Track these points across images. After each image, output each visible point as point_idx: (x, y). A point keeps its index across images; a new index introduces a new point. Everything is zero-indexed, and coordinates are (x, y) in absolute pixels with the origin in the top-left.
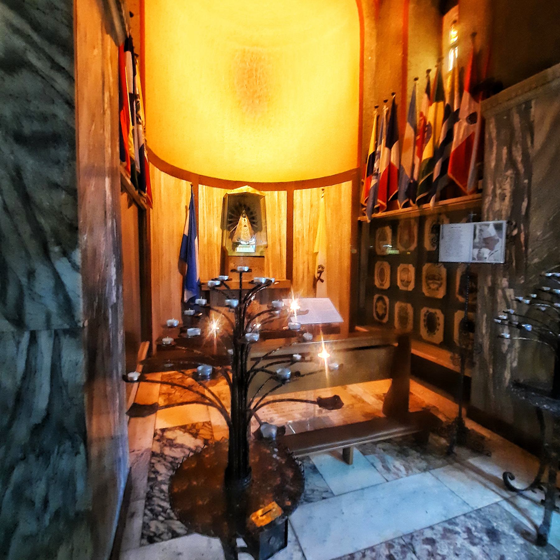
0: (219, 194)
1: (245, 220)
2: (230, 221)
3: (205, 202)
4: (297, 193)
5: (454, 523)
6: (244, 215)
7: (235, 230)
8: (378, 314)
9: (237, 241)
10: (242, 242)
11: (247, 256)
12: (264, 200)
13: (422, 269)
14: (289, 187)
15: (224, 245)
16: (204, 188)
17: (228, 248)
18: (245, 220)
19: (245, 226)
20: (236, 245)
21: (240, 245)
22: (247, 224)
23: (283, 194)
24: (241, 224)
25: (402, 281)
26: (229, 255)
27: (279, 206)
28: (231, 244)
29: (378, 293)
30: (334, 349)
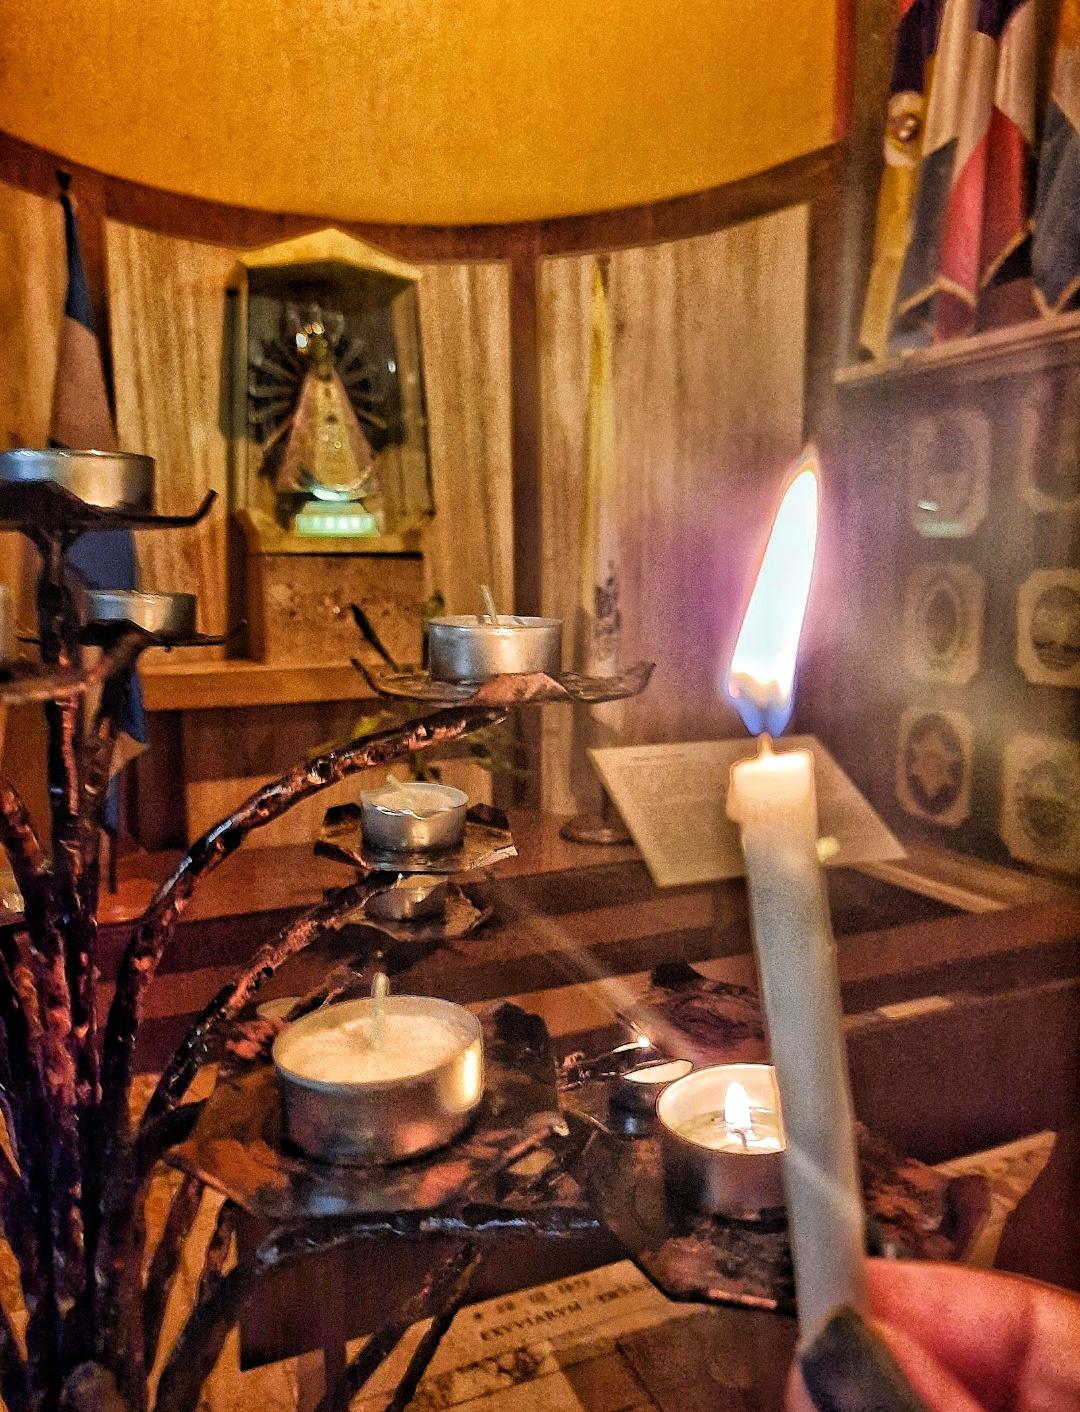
0: (207, 266)
1: (328, 393)
2: (263, 400)
3: (139, 304)
4: (557, 273)
5: (844, 497)
6: (323, 369)
7: (284, 438)
8: (915, 783)
9: (296, 487)
10: (318, 493)
11: (337, 557)
12: (414, 310)
13: (146, 1386)
14: (523, 242)
15: (240, 505)
16: (134, 242)
17: (258, 517)
18: (328, 393)
19: (332, 419)
20: (290, 505)
21: (310, 506)
22: (338, 411)
23: (495, 277)
24: (311, 413)
25: (1039, 645)
26: (265, 548)
27: (477, 331)
28: (270, 498)
29: (945, 830)
30: (658, 1001)
